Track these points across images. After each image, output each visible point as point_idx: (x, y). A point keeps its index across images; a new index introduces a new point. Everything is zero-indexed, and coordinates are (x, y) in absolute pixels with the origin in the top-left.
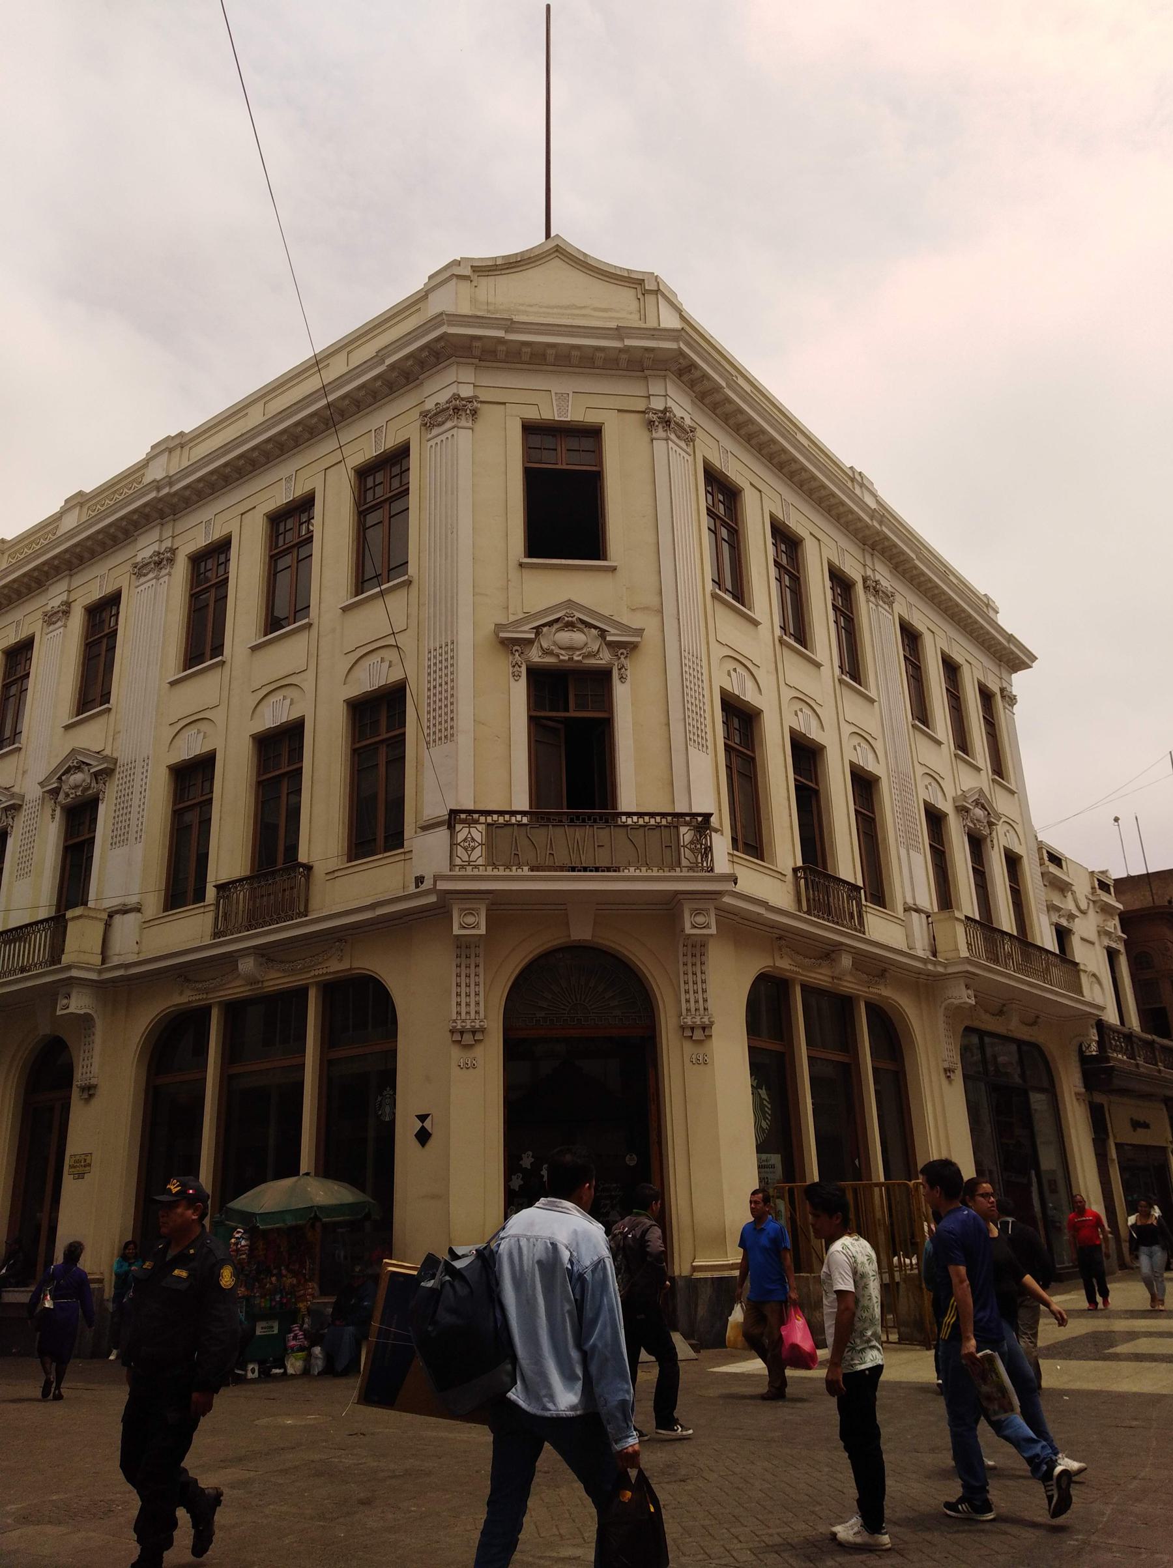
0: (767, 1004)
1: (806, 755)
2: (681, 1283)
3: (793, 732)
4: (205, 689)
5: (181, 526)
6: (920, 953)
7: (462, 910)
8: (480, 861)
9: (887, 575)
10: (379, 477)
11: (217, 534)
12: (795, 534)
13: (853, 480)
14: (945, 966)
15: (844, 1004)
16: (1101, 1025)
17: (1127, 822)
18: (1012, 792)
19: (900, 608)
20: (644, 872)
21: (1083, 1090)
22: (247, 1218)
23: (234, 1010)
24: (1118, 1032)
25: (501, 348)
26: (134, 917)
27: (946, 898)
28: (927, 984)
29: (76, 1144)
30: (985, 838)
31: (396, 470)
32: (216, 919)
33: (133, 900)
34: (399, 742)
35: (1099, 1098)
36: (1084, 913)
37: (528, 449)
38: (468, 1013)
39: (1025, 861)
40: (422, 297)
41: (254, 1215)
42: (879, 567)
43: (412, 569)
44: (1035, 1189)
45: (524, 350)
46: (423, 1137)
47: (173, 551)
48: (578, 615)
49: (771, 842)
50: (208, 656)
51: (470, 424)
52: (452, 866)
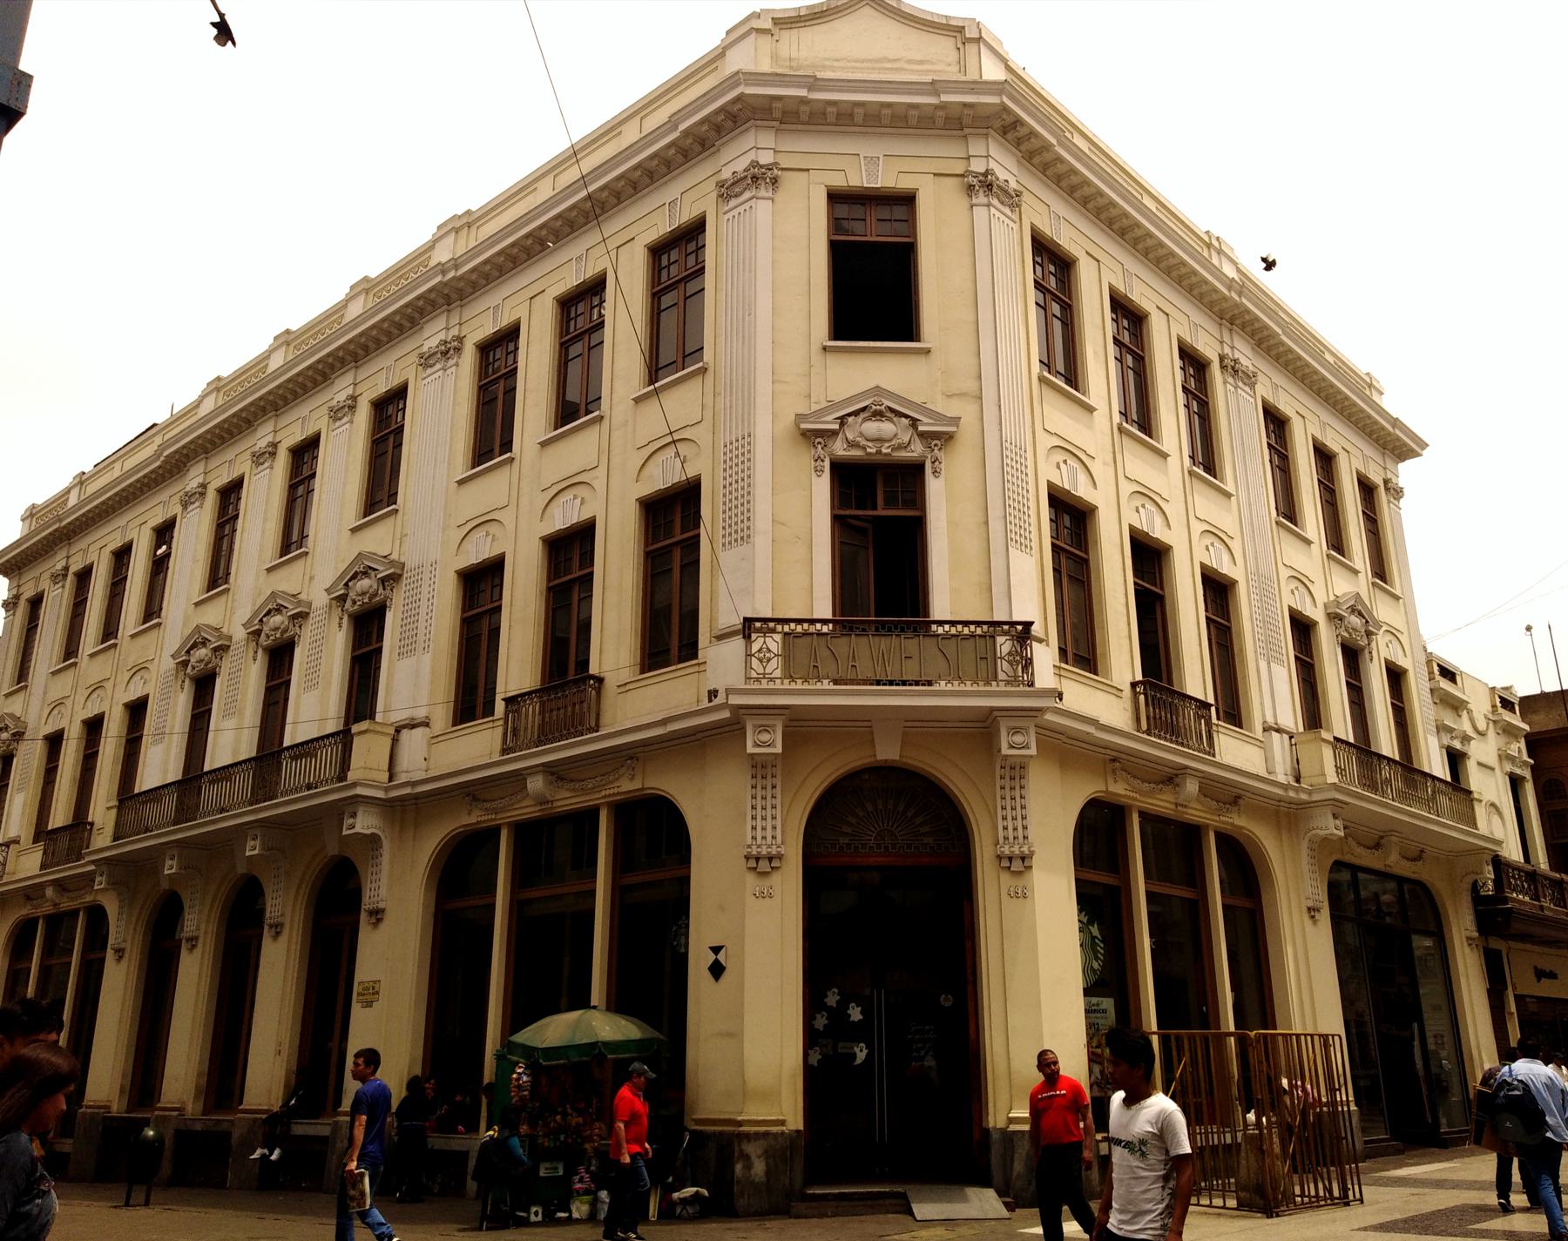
0: (1098, 835)
1: (1149, 557)
2: (995, 1136)
3: (1133, 531)
4: (494, 487)
5: (469, 312)
6: (1281, 778)
7: (755, 726)
8: (778, 673)
9: (1249, 353)
10: (674, 255)
11: (505, 321)
12: (1139, 308)
13: (1209, 246)
14: (1310, 793)
15: (1191, 834)
16: (1498, 863)
17: (1540, 632)
18: (1397, 598)
19: (1263, 390)
20: (956, 686)
21: (1476, 934)
22: (529, 1052)
23: (522, 830)
24: (1519, 870)
25: (804, 108)
26: (423, 735)
27: (1313, 715)
28: (1288, 814)
29: (364, 971)
30: (1363, 649)
31: (692, 247)
32: (505, 734)
33: (420, 714)
34: (693, 545)
35: (1496, 944)
36: (1482, 734)
37: (835, 224)
38: (764, 838)
39: (1411, 676)
40: (720, 54)
41: (535, 1049)
42: (1239, 343)
43: (708, 355)
44: (1416, 1043)
45: (829, 109)
46: (717, 970)
47: (460, 339)
48: (887, 403)
49: (1106, 655)
50: (497, 450)
51: (770, 194)
52: (748, 678)
